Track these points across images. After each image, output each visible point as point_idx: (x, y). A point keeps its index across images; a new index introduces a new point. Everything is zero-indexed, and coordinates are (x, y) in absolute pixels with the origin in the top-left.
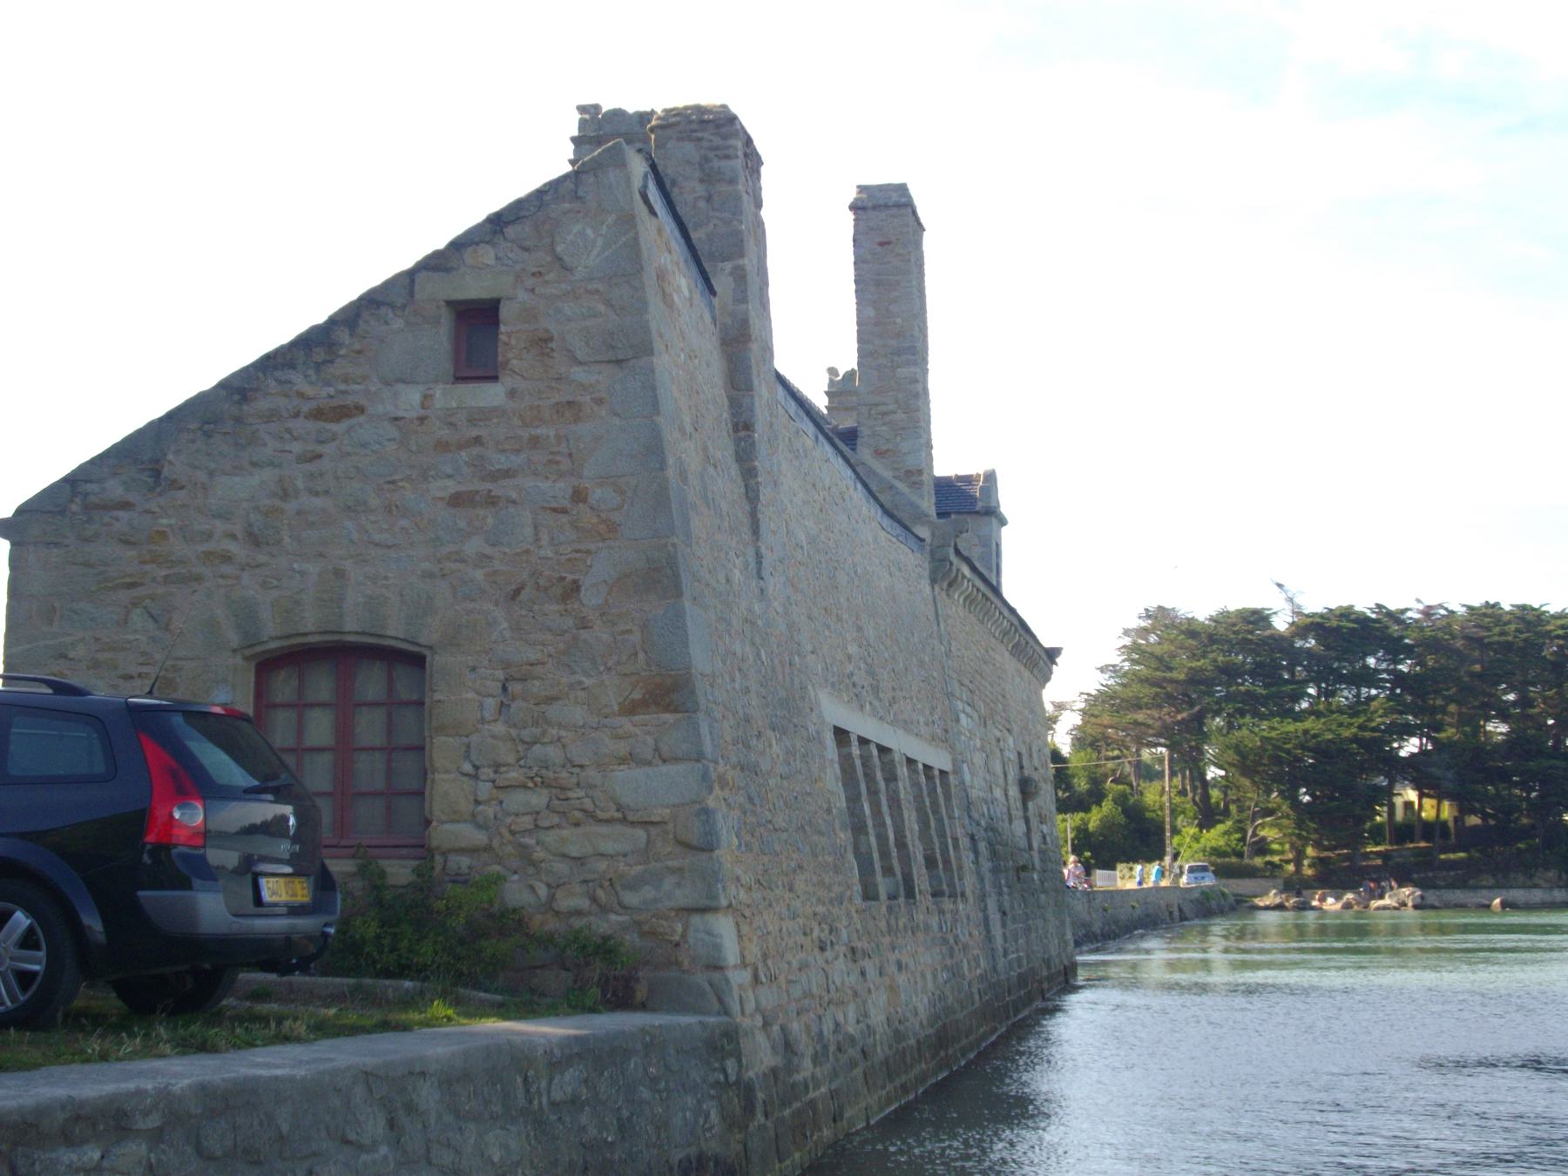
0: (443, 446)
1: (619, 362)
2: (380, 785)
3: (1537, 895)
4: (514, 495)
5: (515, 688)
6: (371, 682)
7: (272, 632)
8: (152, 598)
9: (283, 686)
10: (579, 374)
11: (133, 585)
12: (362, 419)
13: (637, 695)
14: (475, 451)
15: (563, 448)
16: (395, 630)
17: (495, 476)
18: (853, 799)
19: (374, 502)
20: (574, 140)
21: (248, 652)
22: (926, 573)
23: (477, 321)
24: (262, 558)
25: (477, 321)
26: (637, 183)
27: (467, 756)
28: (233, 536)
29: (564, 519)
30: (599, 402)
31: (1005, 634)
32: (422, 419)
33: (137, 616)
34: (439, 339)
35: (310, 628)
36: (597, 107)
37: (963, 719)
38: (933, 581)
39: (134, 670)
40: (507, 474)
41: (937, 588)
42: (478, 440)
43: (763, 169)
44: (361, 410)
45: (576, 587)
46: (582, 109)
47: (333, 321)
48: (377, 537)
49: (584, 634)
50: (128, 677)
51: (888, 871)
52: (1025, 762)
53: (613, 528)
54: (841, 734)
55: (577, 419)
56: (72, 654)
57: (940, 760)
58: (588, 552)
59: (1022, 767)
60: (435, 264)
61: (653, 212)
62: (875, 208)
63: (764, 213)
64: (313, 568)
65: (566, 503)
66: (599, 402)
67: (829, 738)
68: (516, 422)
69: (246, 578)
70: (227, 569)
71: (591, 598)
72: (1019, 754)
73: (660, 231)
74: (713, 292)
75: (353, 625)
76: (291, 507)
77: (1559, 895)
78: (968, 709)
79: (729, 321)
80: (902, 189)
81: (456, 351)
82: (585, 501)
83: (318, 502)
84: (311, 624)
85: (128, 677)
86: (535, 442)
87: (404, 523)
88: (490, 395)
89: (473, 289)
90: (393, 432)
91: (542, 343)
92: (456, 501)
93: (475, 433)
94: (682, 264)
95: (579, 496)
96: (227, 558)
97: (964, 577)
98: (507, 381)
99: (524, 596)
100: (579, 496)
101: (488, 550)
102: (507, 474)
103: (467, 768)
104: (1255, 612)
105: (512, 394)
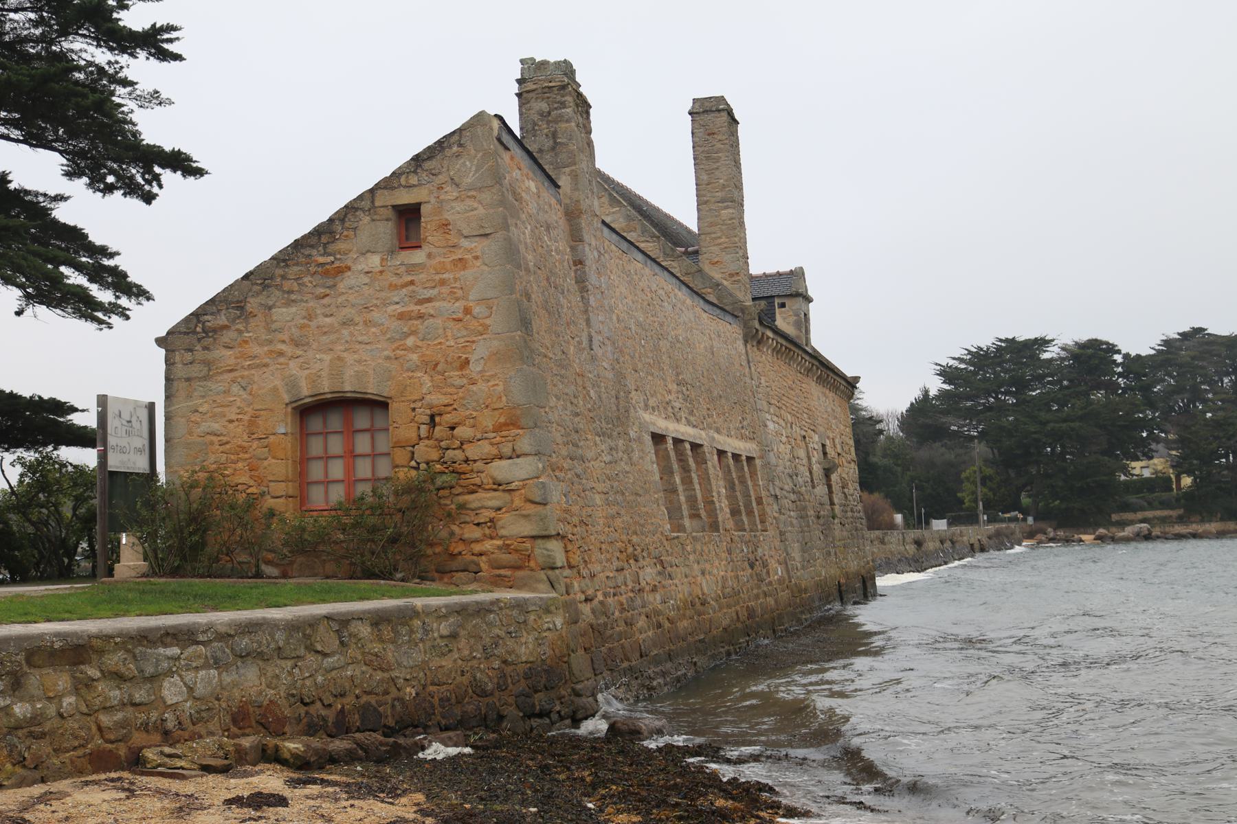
0: (393, 287)
1: (486, 235)
2: (369, 475)
3: (1213, 527)
4: (432, 312)
5: (437, 419)
6: (362, 419)
7: (306, 391)
8: (242, 377)
9: (316, 423)
10: (465, 243)
11: (231, 371)
12: (349, 273)
13: (502, 420)
14: (411, 288)
15: (457, 285)
16: (372, 388)
17: (421, 302)
18: (666, 471)
19: (357, 319)
20: (518, 81)
21: (295, 405)
22: (741, 337)
23: (409, 215)
24: (299, 352)
25: (409, 215)
26: (496, 133)
27: (412, 458)
28: (284, 342)
29: (461, 324)
30: (476, 258)
31: (809, 370)
32: (381, 272)
33: (235, 389)
34: (386, 230)
35: (327, 390)
36: (533, 59)
37: (771, 425)
38: (746, 342)
39: (234, 417)
40: (429, 300)
41: (749, 346)
42: (412, 283)
43: (591, 111)
44: (349, 268)
45: (467, 362)
46: (522, 61)
47: (331, 220)
48: (360, 339)
49: (474, 388)
50: (231, 421)
51: (695, 516)
52: (828, 450)
53: (486, 327)
54: (658, 438)
55: (464, 268)
56: (201, 410)
57: (744, 447)
58: (473, 342)
59: (825, 454)
60: (386, 184)
61: (507, 149)
62: (705, 112)
63: (593, 136)
64: (327, 357)
65: (460, 315)
66: (476, 258)
67: (648, 439)
68: (432, 271)
69: (292, 364)
70: (282, 360)
71: (475, 368)
72: (824, 446)
73: (512, 158)
74: (559, 187)
75: (349, 386)
76: (313, 324)
77: (1231, 525)
78: (775, 419)
79: (568, 201)
80: (722, 99)
81: (399, 234)
82: (470, 313)
83: (328, 320)
84: (326, 387)
85: (231, 421)
86: (443, 283)
87: (373, 330)
88: (418, 257)
89: (405, 198)
90: (367, 280)
91: (445, 225)
92: (401, 316)
93: (409, 278)
94: (531, 175)
95: (467, 311)
96: (281, 354)
97: (768, 338)
98: (426, 249)
99: (439, 368)
100: (467, 311)
101: (420, 343)
102: (429, 300)
103: (413, 463)
104: (1094, 344)
105: (429, 256)
